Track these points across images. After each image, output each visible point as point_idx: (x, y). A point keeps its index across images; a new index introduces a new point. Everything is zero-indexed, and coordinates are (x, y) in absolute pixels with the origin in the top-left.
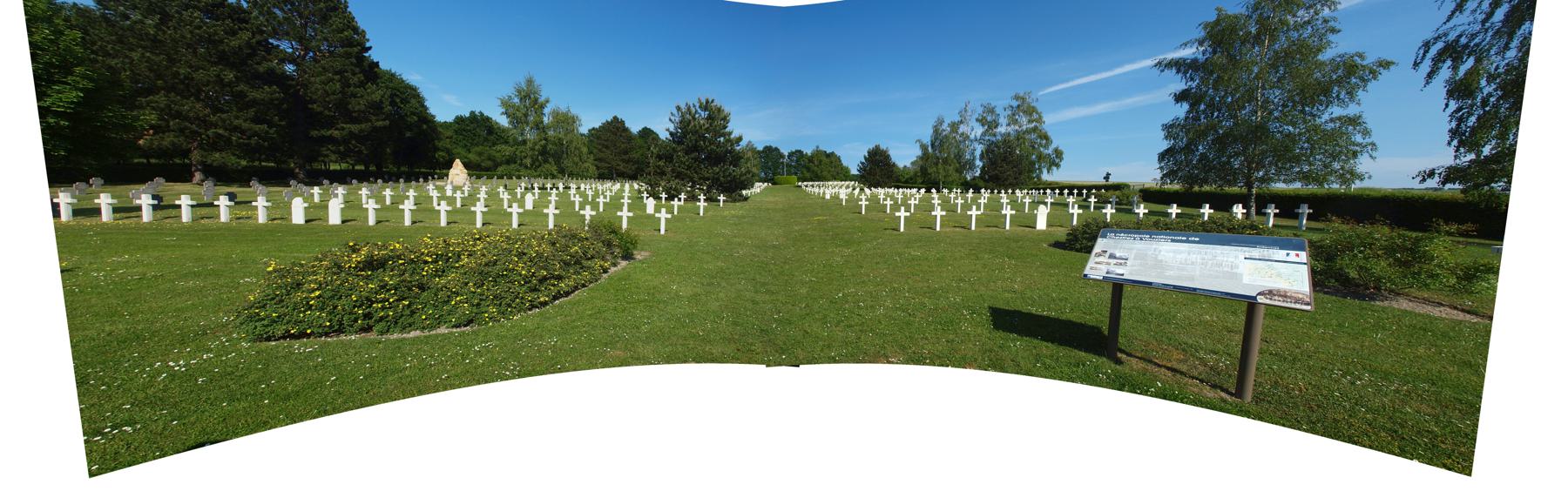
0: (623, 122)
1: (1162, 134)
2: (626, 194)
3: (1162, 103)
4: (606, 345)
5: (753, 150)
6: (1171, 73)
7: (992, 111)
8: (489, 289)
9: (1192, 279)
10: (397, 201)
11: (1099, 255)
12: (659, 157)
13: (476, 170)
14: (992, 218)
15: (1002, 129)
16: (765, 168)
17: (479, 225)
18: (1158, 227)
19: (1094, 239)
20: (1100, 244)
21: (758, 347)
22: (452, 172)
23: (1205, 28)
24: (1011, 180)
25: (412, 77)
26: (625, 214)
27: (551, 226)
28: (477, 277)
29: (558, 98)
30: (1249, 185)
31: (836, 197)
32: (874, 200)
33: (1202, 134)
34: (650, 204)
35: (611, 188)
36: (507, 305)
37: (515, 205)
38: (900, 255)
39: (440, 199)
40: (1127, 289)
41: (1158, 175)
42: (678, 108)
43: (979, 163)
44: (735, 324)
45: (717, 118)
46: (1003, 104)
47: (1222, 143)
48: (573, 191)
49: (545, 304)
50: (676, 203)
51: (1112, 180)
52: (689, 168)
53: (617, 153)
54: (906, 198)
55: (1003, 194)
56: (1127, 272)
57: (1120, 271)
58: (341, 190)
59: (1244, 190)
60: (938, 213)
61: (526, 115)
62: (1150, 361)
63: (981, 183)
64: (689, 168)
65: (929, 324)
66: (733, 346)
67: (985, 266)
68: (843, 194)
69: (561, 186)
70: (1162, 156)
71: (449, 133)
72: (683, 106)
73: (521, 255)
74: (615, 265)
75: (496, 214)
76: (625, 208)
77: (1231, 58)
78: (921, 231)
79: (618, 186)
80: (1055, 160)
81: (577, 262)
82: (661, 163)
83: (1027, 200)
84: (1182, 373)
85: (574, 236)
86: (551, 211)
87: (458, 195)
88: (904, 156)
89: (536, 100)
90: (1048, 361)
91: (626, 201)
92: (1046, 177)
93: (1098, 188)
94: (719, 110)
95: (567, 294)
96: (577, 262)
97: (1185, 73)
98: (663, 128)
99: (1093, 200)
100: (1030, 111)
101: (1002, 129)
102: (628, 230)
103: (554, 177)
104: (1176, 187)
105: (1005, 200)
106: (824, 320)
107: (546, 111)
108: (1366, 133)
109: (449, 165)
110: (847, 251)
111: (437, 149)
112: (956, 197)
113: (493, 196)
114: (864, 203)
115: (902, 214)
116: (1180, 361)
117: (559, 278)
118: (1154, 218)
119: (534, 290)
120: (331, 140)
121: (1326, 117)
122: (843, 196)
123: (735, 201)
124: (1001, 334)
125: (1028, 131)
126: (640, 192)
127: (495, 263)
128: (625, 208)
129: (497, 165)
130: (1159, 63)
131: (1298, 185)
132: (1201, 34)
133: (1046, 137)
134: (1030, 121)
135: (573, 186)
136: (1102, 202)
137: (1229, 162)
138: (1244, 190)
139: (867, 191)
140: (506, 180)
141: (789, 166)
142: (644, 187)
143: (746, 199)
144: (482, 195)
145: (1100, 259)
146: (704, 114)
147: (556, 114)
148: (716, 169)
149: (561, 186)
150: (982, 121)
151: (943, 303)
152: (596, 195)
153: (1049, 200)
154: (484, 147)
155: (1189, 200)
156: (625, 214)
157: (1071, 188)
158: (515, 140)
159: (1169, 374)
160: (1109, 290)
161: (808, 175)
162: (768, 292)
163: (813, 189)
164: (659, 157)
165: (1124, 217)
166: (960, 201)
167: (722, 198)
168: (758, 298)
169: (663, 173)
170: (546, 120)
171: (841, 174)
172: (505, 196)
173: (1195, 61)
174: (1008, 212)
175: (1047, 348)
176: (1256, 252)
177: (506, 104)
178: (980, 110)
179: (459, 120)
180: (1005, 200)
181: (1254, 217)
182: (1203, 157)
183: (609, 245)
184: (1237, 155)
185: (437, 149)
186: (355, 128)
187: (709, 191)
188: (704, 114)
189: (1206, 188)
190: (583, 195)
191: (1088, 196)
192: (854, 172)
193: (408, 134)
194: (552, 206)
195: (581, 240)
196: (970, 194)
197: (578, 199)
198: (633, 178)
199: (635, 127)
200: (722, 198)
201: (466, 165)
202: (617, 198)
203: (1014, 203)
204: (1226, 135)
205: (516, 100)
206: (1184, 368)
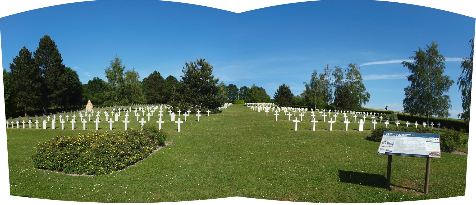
0: (159, 74)
1: (404, 92)
2: (161, 111)
3: (402, 80)
4: (151, 190)
5: (224, 86)
6: (406, 68)
7: (340, 70)
8: (102, 159)
9: (413, 151)
10: (70, 119)
11: (383, 143)
12: (177, 91)
13: (96, 104)
14: (339, 125)
15: (344, 80)
16: (229, 95)
17: (97, 129)
18: (402, 130)
19: (381, 136)
20: (384, 138)
21: (226, 189)
22: (88, 106)
23: (416, 53)
24: (348, 106)
25: (74, 68)
26: (160, 122)
27: (126, 129)
28: (96, 153)
29: (128, 66)
30: (427, 116)
31: (263, 111)
32: (282, 113)
33: (415, 94)
34: (173, 116)
35: (153, 108)
36: (108, 167)
37: (111, 119)
38: (295, 143)
39: (83, 118)
40: (393, 157)
41: (403, 109)
42: (187, 65)
43: (334, 96)
44: (215, 178)
45: (206, 69)
46: (344, 67)
47: (420, 98)
48: (136, 111)
49: (123, 168)
50: (185, 115)
51: (389, 109)
52: (192, 96)
53: (158, 90)
54: (298, 113)
55: (345, 113)
56: (394, 150)
57: (391, 150)
58: (55, 116)
59: (426, 117)
60: (314, 121)
61: (115, 76)
62: (401, 187)
63: (335, 107)
64: (192, 96)
65: (310, 180)
66: (214, 190)
67: (336, 149)
68: (267, 110)
69: (130, 109)
70: (405, 101)
71: (86, 89)
72: (189, 63)
73: (113, 143)
74: (155, 149)
75: (104, 124)
76: (160, 119)
77: (423, 67)
78: (305, 131)
79: (157, 107)
80: (366, 98)
81: (137, 147)
82: (178, 94)
83: (355, 117)
84: (410, 189)
85: (136, 134)
86: (126, 121)
87: (89, 116)
88: (297, 91)
89: (120, 67)
90: (364, 195)
91: (161, 115)
92: (363, 106)
93: (383, 112)
94: (207, 65)
95: (133, 163)
96: (137, 147)
97: (411, 69)
98: (179, 75)
99: (381, 118)
100: (357, 73)
101: (344, 80)
102: (162, 130)
103: (127, 105)
104: (408, 114)
105: (345, 116)
106: (257, 176)
107: (124, 72)
108: (450, 101)
109: (86, 103)
110: (268, 140)
111: (82, 97)
112: (323, 113)
113: (102, 115)
114: (277, 115)
115: (296, 121)
116: (410, 184)
117: (130, 155)
118: (402, 127)
119: (119, 160)
120: (52, 98)
121: (443, 95)
122: (266, 111)
123: (215, 113)
124: (344, 184)
125: (356, 83)
126: (168, 110)
127: (103, 147)
128: (160, 119)
129: (104, 101)
130: (403, 63)
131: (437, 116)
132: (415, 56)
133: (363, 87)
134: (357, 78)
135: (136, 108)
136: (385, 119)
137: (422, 106)
138: (426, 117)
139: (278, 108)
140: (107, 108)
141: (240, 95)
142: (170, 107)
143: (220, 112)
144: (98, 116)
145: (384, 145)
146: (200, 67)
147: (128, 73)
148: (206, 96)
149: (130, 109)
150: (335, 75)
151: (316, 169)
152: (146, 113)
153: (364, 117)
154: (107, 93)
155: (412, 120)
156: (160, 122)
157: (373, 112)
158: (111, 88)
159: (406, 190)
160: (387, 157)
161: (249, 99)
162: (232, 159)
163: (252, 106)
164: (177, 91)
165: (392, 126)
166: (325, 116)
167: (209, 112)
168: (227, 163)
169: (179, 100)
170: (124, 77)
171: (266, 99)
172: (107, 115)
173: (413, 65)
174: (347, 122)
175: (363, 188)
176: (429, 139)
177: (107, 72)
178: (334, 69)
179: (90, 82)
180: (345, 116)
181: (428, 127)
182: (416, 103)
183: (153, 138)
184: (424, 104)
185: (82, 97)
186: (58, 92)
187: (202, 108)
188: (200, 67)
189: (417, 115)
190: (140, 113)
191: (380, 116)
192: (272, 98)
193: (73, 92)
194: (126, 119)
195: (139, 136)
196: (330, 112)
197: (138, 115)
198: (164, 102)
199: (165, 76)
200: (209, 112)
201: (93, 103)
202: (157, 113)
203: (350, 118)
204: (422, 96)
205: (111, 69)
206: (410, 187)
